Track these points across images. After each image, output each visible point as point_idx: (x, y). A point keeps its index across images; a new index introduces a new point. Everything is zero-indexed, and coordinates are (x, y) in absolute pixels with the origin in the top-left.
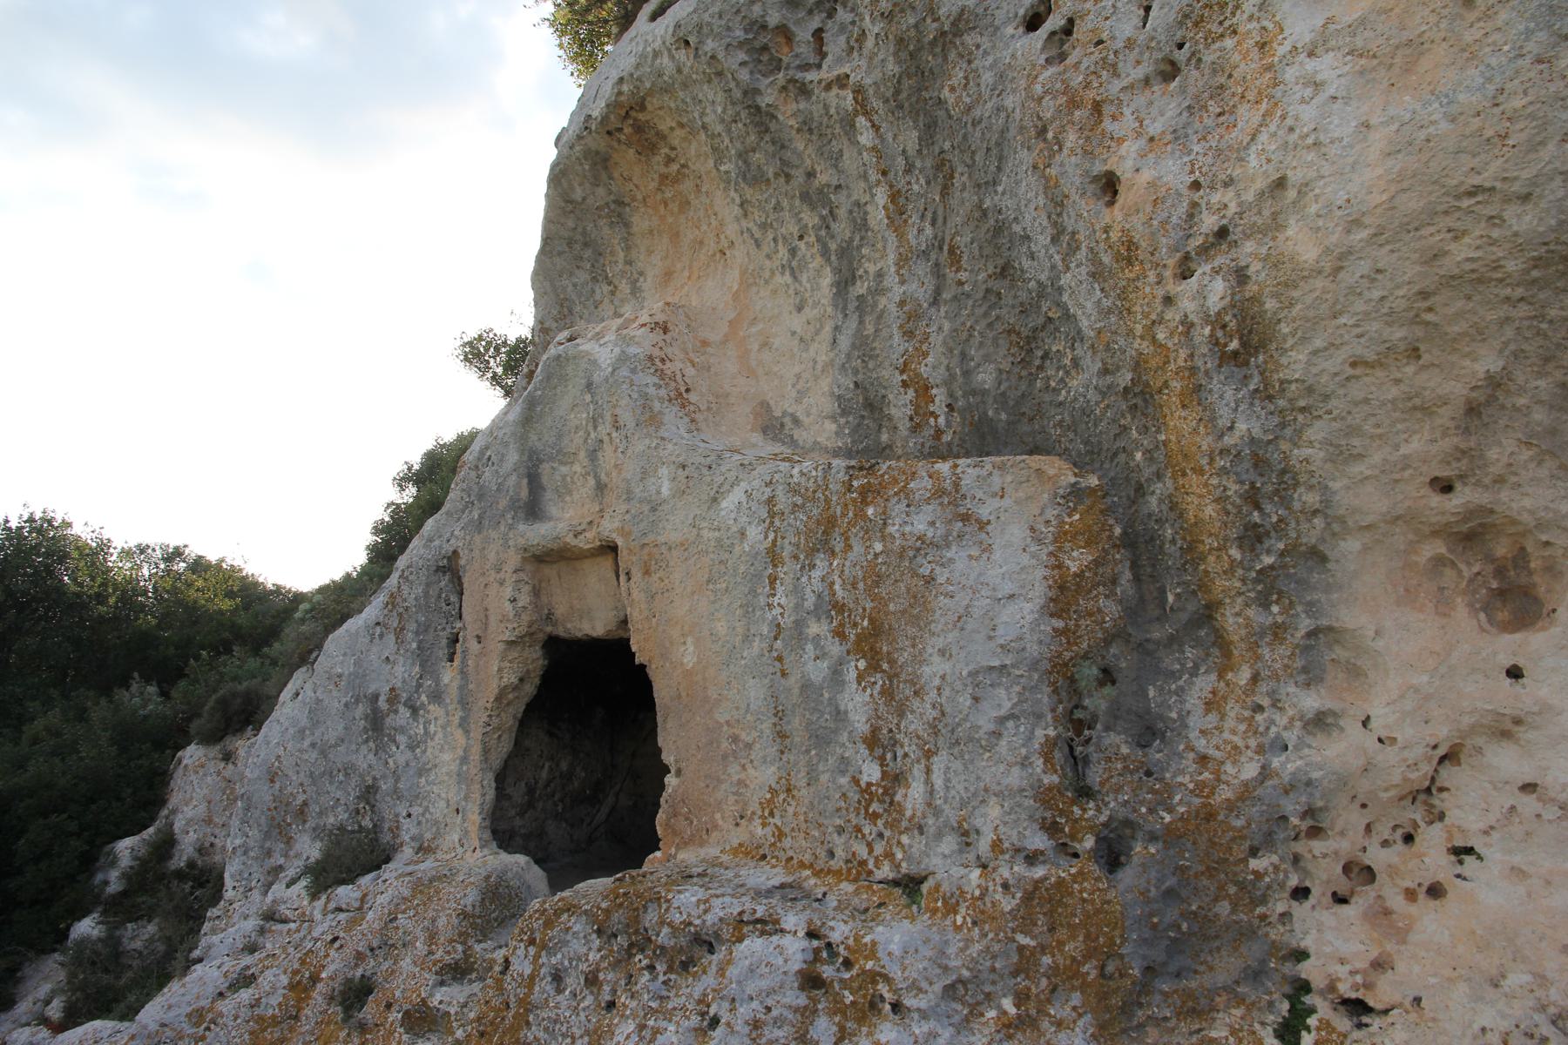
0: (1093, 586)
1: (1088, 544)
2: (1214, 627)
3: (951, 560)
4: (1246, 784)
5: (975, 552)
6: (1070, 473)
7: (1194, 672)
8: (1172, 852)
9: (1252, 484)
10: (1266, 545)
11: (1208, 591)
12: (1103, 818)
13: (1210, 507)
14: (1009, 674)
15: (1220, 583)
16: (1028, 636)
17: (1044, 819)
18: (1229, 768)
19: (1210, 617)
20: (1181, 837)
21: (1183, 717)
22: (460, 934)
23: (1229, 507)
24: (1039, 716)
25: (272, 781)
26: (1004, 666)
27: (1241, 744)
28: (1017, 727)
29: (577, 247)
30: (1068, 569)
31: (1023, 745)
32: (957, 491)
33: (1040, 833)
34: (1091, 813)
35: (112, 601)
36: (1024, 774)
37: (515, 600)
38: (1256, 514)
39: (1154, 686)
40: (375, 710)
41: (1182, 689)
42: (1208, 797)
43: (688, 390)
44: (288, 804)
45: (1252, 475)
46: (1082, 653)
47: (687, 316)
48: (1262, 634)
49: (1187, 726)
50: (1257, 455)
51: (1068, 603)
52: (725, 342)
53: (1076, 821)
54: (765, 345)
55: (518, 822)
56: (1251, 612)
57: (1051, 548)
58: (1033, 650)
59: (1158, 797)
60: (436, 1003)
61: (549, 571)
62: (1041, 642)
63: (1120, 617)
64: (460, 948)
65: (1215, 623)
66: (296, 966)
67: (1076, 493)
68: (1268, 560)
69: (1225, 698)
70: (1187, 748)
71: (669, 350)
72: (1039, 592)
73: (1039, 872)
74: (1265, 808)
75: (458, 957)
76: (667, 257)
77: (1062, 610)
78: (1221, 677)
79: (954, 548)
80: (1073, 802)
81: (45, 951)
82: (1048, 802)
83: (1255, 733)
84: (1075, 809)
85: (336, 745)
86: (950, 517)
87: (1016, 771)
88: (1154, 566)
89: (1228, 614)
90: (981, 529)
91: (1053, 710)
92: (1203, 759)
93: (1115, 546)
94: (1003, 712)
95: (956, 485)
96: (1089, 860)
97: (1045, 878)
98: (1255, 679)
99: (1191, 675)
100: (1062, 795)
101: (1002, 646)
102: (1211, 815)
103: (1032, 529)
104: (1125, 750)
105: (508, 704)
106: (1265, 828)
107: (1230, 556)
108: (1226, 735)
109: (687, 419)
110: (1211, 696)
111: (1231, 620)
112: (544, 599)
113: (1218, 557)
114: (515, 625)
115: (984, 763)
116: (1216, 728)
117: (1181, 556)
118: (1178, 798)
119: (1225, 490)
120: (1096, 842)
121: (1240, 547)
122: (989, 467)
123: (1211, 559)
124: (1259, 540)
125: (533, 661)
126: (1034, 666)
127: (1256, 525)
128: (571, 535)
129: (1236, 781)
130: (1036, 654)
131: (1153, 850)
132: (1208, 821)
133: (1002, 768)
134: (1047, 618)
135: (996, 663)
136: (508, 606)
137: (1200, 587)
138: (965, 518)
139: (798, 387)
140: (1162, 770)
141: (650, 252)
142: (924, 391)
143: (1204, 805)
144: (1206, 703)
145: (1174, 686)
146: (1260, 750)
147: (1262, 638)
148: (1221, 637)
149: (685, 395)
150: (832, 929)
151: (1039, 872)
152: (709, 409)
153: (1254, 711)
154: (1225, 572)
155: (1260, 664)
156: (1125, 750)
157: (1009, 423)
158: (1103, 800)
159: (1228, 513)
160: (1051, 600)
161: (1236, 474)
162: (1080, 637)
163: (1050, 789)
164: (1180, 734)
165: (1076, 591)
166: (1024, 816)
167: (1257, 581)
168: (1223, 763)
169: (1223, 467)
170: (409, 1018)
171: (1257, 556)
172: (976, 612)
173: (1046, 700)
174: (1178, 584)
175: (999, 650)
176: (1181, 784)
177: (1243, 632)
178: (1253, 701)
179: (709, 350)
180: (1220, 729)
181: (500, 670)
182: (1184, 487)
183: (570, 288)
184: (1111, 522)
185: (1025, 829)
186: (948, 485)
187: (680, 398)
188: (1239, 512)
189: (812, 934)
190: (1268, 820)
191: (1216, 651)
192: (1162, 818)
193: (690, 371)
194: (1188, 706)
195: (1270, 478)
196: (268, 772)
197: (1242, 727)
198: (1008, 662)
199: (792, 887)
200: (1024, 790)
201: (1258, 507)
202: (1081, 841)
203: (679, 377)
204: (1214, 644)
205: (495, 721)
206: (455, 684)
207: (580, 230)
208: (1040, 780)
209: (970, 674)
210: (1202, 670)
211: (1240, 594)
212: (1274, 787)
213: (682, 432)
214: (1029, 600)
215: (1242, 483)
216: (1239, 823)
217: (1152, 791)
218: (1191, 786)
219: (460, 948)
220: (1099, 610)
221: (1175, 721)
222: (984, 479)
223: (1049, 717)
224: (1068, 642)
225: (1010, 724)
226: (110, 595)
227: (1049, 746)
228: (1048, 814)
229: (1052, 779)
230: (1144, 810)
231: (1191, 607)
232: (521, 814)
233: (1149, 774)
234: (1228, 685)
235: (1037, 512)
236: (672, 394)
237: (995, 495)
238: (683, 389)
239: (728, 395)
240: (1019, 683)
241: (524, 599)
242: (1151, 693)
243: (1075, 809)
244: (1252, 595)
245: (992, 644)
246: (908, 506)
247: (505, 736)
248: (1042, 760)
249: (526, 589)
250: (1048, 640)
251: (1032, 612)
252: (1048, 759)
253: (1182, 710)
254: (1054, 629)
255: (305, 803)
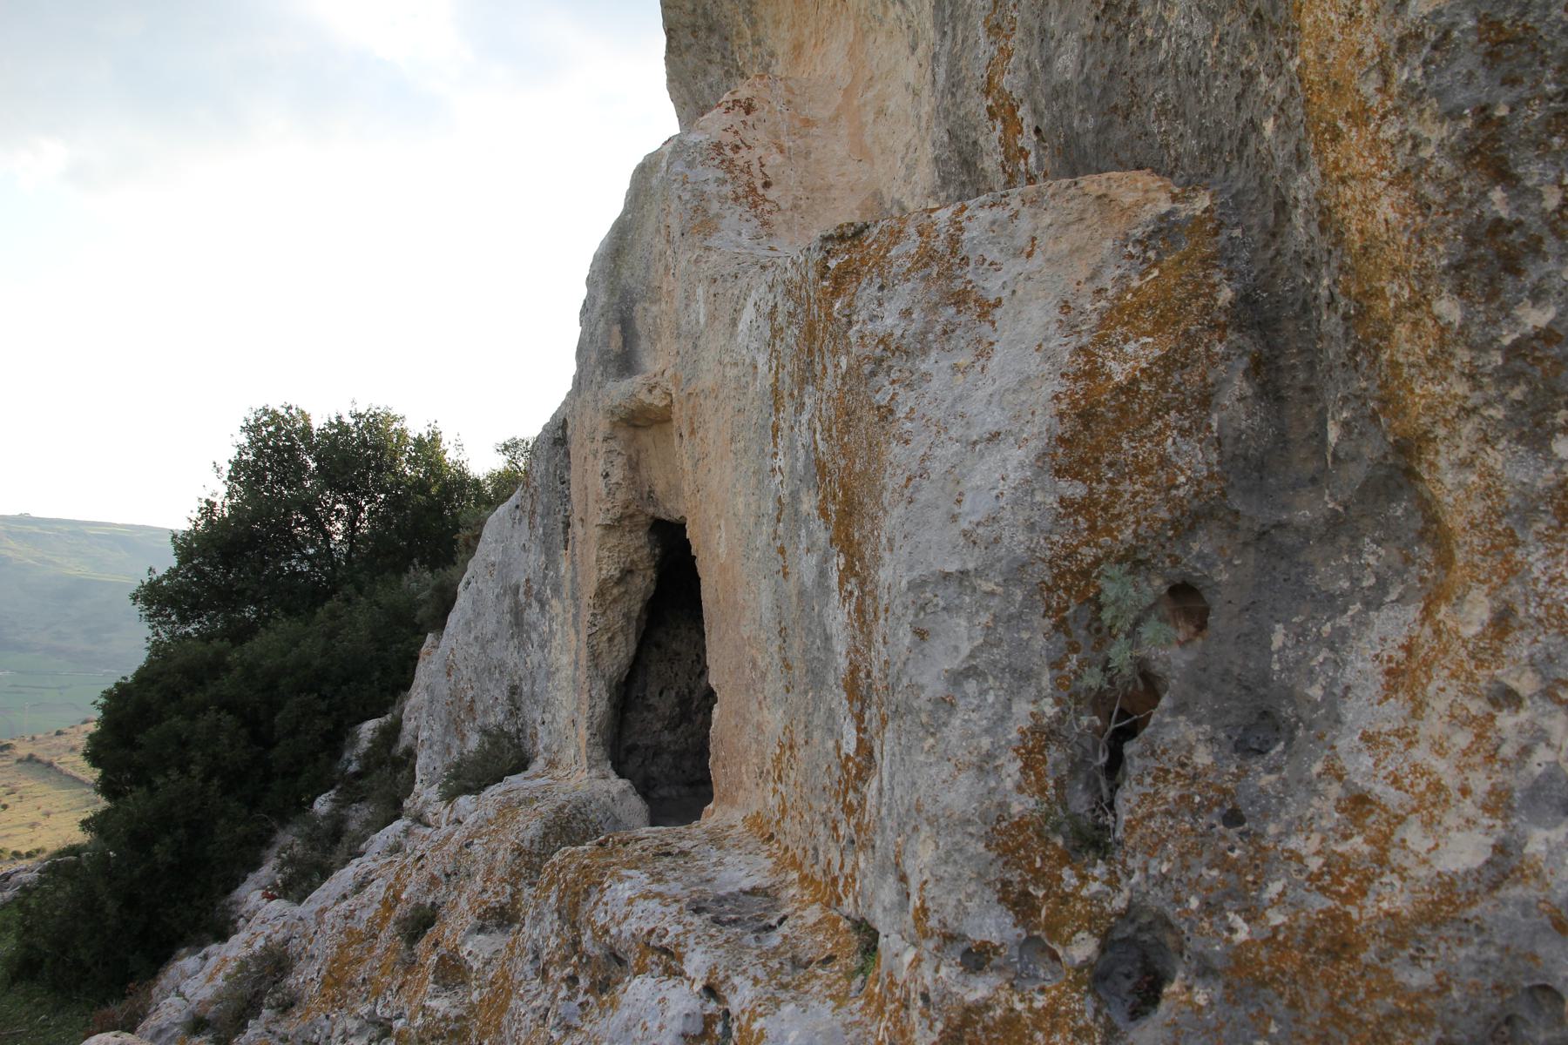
0: (1155, 411)
1: (1159, 326)
2: (1419, 496)
3: (926, 377)
4: (1448, 884)
5: (964, 359)
6: (1164, 196)
7: (1373, 602)
8: (1240, 1013)
9: (1483, 113)
10: (1529, 280)
11: (1401, 411)
12: (1119, 903)
13: (1385, 201)
14: (974, 590)
15: (1424, 389)
16: (1007, 514)
17: (1006, 884)
18: (1414, 835)
19: (1411, 474)
20: (1264, 984)
21: (1337, 695)
22: (513, 874)
23: (1428, 190)
24: (1024, 676)
25: (449, 675)
26: (964, 573)
27: (1450, 780)
28: (983, 693)
29: (702, 34)
30: (1109, 377)
31: (987, 731)
32: (954, 253)
33: (998, 909)
34: (1095, 887)
35: (434, 491)
36: (980, 789)
37: (607, 475)
38: (1497, 194)
39: (1287, 623)
40: (517, 603)
41: (1343, 633)
42: (1347, 898)
43: (767, 185)
44: (461, 699)
45: (1484, 87)
46: (1121, 550)
47: (790, 90)
48: (1528, 513)
49: (1338, 721)
50: (1496, 25)
51: (1098, 448)
52: (835, 118)
53: (1065, 899)
54: (881, 112)
55: (667, 737)
56: (1494, 458)
57: (1085, 339)
58: (1017, 542)
59: (1232, 877)
60: (465, 953)
61: (645, 438)
62: (1031, 527)
63: (1211, 476)
64: (508, 889)
65: (1420, 487)
66: (392, 881)
67: (1166, 229)
68: (1536, 318)
69: (1427, 664)
70: (1327, 770)
71: (749, 136)
72: (1040, 425)
73: (979, 989)
74: (1492, 953)
75: (504, 901)
76: (794, 25)
77: (1083, 462)
78: (1428, 613)
79: (933, 354)
80: (1065, 858)
81: (284, 821)
82: (1013, 851)
83: (1491, 757)
84: (1066, 873)
85: (493, 640)
86: (936, 299)
87: (965, 780)
88: (1311, 366)
89: (1443, 463)
90: (983, 315)
91: (1056, 665)
92: (1359, 804)
93: (1215, 326)
94: (955, 663)
95: (954, 241)
96: (1076, 984)
97: (986, 1006)
98: (1502, 622)
99: (1368, 605)
100: (1046, 841)
101: (965, 534)
102: (1345, 945)
103: (1065, 307)
104: (1202, 758)
105: (615, 601)
106: (1491, 1004)
107: (1436, 319)
108: (1420, 754)
109: (756, 222)
110: (1401, 655)
111: (1449, 479)
112: (644, 472)
113: (1415, 324)
114: (609, 505)
115: (922, 758)
116: (1400, 734)
117: (1347, 333)
118: (1274, 888)
119: (1415, 147)
120: (1103, 949)
121: (1460, 291)
122: (1015, 203)
123: (1402, 331)
124: (1513, 267)
125: (636, 550)
126: (1016, 572)
127: (1498, 227)
128: (645, 391)
129: (1422, 872)
130: (1020, 551)
131: (1201, 999)
132: (1337, 958)
133: (948, 768)
134: (1047, 478)
135: (953, 567)
136: (601, 482)
137: (1384, 402)
138: (959, 299)
139: (907, 160)
140: (1266, 813)
141: (777, 23)
142: (1004, 111)
143: (1332, 917)
144: (1389, 672)
145: (1327, 628)
146: (1498, 803)
147: (1525, 522)
148: (1435, 520)
149: (761, 191)
150: (734, 989)
151: (979, 989)
152: (795, 207)
153: (1494, 702)
154: (1431, 361)
155: (1516, 588)
156: (1202, 758)
157: (1099, 131)
158: (1124, 863)
159: (1425, 206)
160: (1061, 440)
161: (1439, 94)
162: (1119, 516)
163: (1020, 826)
164: (1321, 737)
165: (1117, 422)
166: (967, 873)
167: (1507, 376)
168: (1401, 820)
169: (1410, 85)
170: (444, 965)
171: (1506, 309)
172: (936, 468)
173: (1039, 642)
174: (1345, 400)
175: (962, 541)
176: (1296, 856)
177: (1478, 508)
178: (1493, 679)
179: (814, 131)
180: (1408, 738)
181: (599, 560)
182: (1336, 166)
183: (707, 91)
184: (1217, 276)
185: (970, 897)
186: (940, 245)
187: (753, 196)
188: (1453, 197)
189: (711, 991)
190: (1499, 988)
191: (1425, 553)
192: (1232, 930)
193: (775, 159)
194: (1349, 675)
195: (1537, 84)
196: (446, 665)
197: (1462, 739)
198: (971, 566)
199: (767, 895)
200: (969, 822)
201: (1503, 175)
202: (1066, 943)
203: (755, 168)
204: (1421, 536)
205: (601, 621)
206: (569, 576)
207: (699, 11)
208: (1003, 805)
209: (912, 586)
210: (1393, 596)
211: (1470, 412)
212: (1525, 907)
213: (745, 240)
214: (1020, 443)
215: (1454, 115)
216: (1418, 978)
217: (1226, 865)
218: (1315, 864)
219: (508, 889)
220: (1164, 461)
221: (1316, 706)
222: (1003, 226)
223: (1046, 678)
224: (1092, 528)
225: (971, 686)
226: (431, 486)
227: (1042, 736)
228: (1014, 876)
229: (1020, 805)
230: (1194, 903)
231: (1371, 450)
232: (672, 727)
233: (1233, 818)
234: (1437, 633)
235: (1086, 273)
236: (740, 191)
237: (1017, 253)
238: (758, 183)
239: (830, 187)
240: (988, 608)
241: (617, 475)
242: (1278, 640)
243: (1066, 873)
244: (1498, 413)
245: (955, 530)
246: (881, 288)
247: (620, 638)
248: (1019, 763)
249: (619, 461)
250: (1047, 523)
251: (1022, 465)
252: (1031, 760)
253: (1333, 682)
254: (1062, 500)
255: (473, 701)
